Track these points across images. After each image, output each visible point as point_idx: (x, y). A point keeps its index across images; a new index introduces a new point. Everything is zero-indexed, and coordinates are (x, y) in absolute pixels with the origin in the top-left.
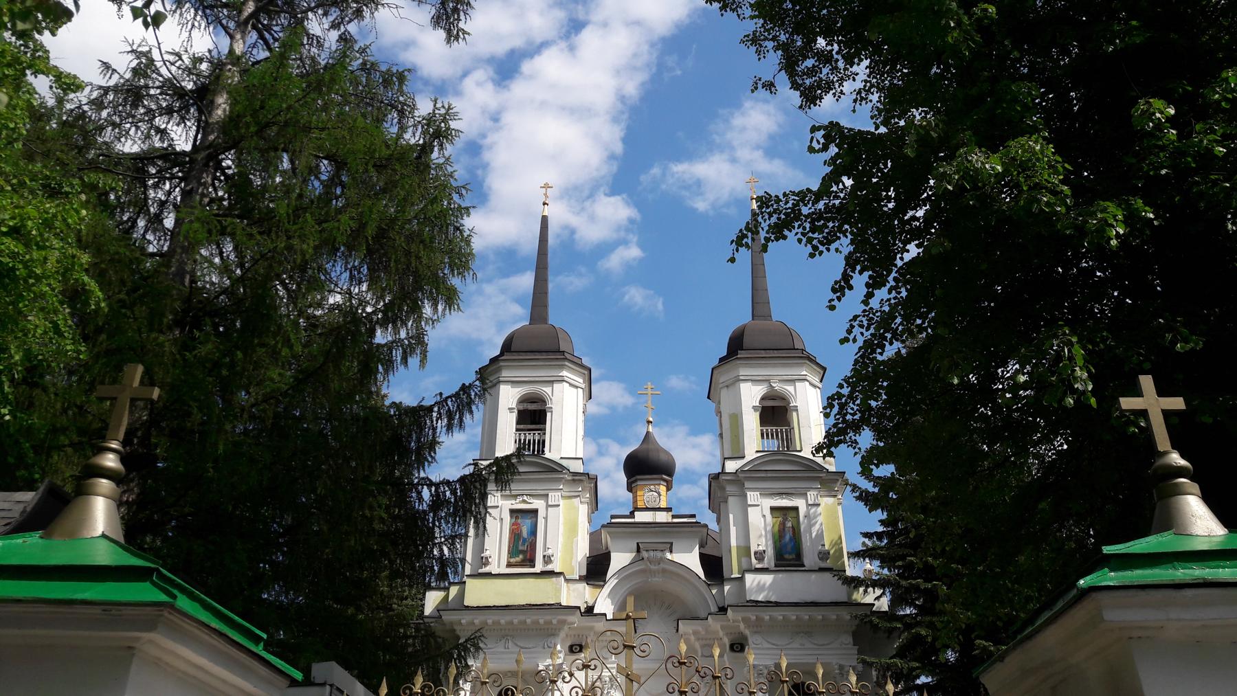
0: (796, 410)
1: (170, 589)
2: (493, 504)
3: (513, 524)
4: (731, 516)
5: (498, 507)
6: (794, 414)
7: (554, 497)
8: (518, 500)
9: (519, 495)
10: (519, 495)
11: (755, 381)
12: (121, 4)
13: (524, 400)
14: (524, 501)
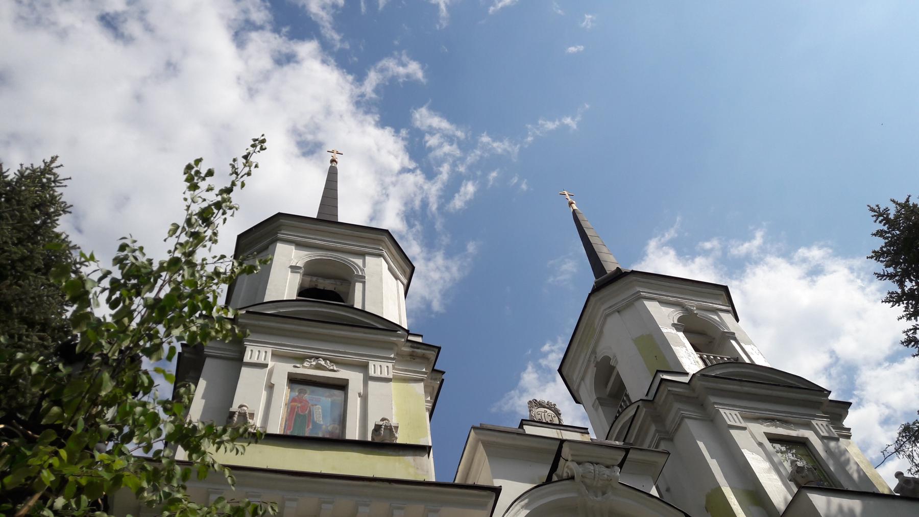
0: (362, 279)
1: (757, 372)
2: (255, 360)
3: (293, 400)
4: (701, 445)
5: (266, 366)
6: (358, 286)
7: (377, 368)
8: (306, 364)
9: (311, 357)
10: (311, 357)
11: (299, 245)
12: (889, 302)
13: (311, 270)
14: (319, 367)
